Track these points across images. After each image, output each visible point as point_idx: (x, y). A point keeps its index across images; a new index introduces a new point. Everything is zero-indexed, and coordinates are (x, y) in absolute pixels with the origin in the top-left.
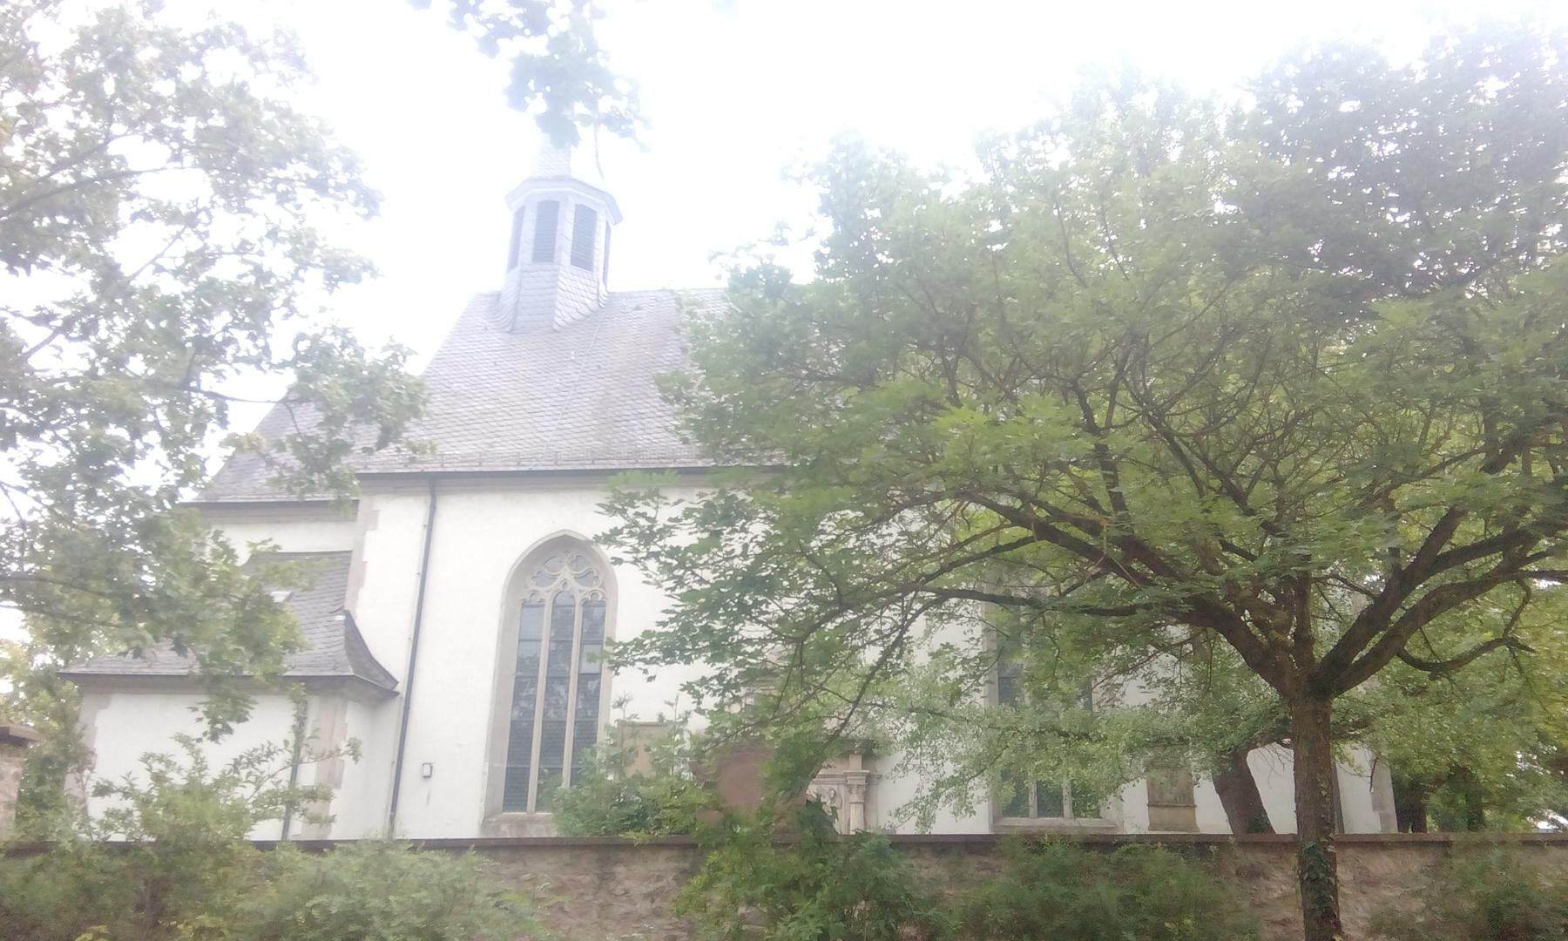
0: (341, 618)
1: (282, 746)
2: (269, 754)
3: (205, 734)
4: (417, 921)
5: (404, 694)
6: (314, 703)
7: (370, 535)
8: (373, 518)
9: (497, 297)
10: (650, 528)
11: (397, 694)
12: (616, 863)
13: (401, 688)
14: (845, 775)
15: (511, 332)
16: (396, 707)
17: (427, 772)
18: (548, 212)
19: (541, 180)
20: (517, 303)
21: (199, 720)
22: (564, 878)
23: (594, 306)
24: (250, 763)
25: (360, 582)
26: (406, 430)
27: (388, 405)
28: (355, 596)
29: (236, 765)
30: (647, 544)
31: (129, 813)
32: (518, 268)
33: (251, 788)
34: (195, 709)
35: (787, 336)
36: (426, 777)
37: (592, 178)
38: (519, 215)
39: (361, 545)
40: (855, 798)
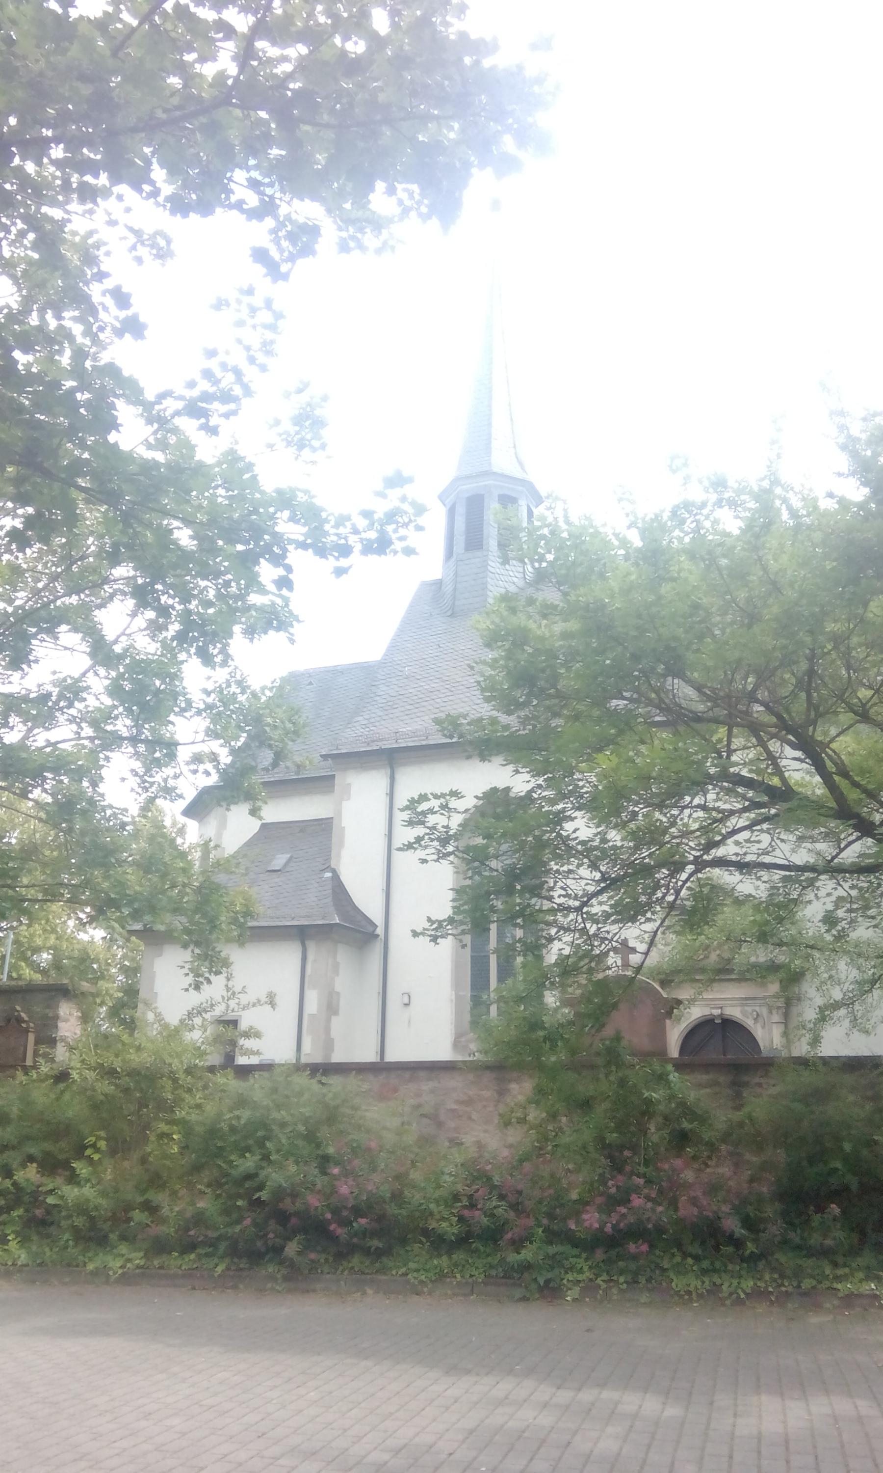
0: (328, 875)
1: (220, 1000)
2: (212, 1005)
3: (190, 985)
4: (301, 1128)
5: (382, 936)
6: (312, 947)
7: (345, 804)
8: (347, 793)
9: (439, 584)
10: (447, 832)
11: (378, 936)
12: (510, 1081)
13: (380, 931)
14: (764, 998)
15: (452, 615)
16: (378, 947)
17: (406, 1001)
18: (475, 506)
19: (468, 477)
20: (455, 590)
21: (187, 975)
22: (471, 1093)
23: (521, 583)
24: (199, 1013)
25: (341, 844)
26: (740, 528)
27: (276, 735)
28: (339, 855)
29: (190, 1015)
30: (444, 846)
31: (633, 950)
32: (453, 559)
33: (200, 1033)
34: (182, 967)
35: (543, 671)
36: (407, 1005)
37: (514, 471)
38: (452, 513)
39: (339, 813)
40: (776, 1017)
